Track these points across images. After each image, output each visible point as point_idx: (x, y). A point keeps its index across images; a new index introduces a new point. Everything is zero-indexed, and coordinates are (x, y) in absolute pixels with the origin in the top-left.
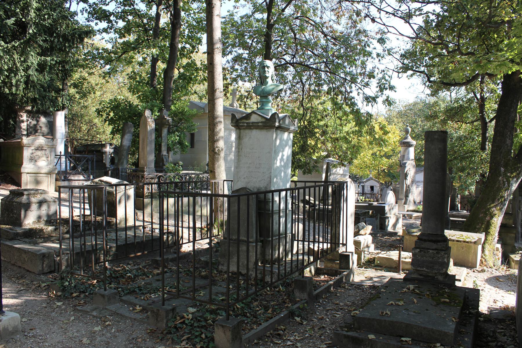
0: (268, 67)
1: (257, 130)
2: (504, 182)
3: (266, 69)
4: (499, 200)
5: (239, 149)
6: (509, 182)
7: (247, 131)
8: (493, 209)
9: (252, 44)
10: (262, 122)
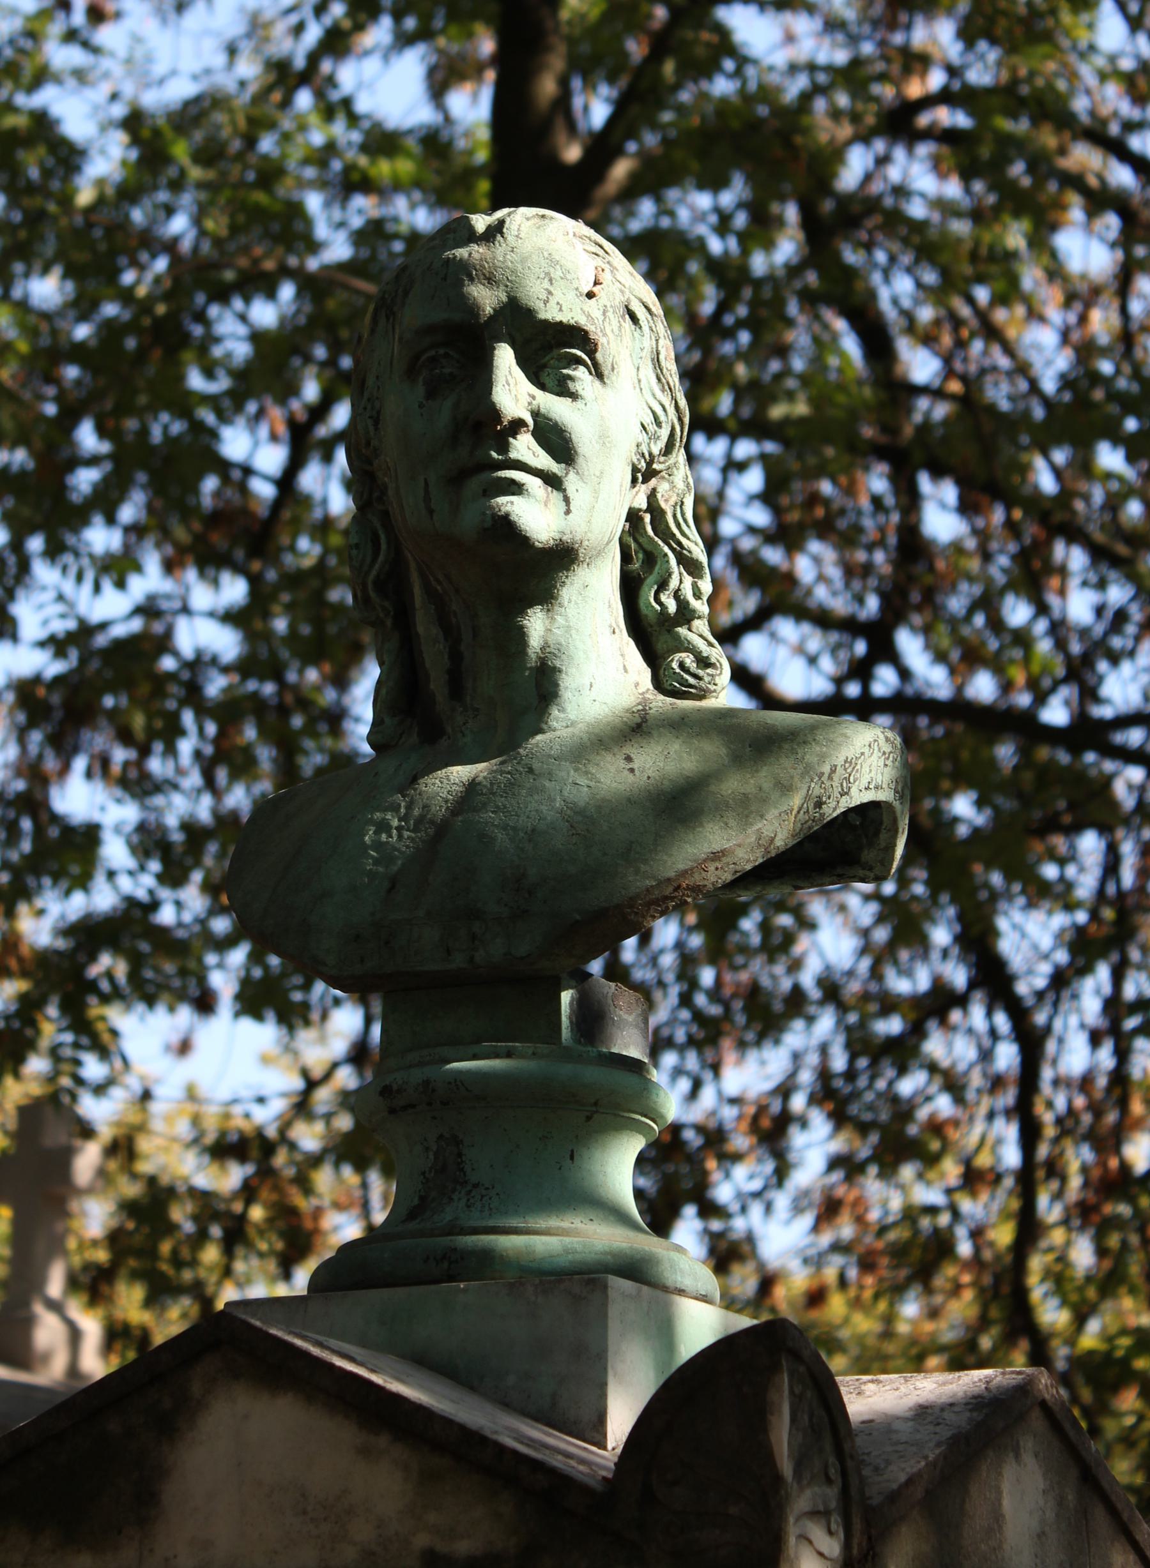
0: (556, 351)
3: (512, 390)
9: (286, 481)
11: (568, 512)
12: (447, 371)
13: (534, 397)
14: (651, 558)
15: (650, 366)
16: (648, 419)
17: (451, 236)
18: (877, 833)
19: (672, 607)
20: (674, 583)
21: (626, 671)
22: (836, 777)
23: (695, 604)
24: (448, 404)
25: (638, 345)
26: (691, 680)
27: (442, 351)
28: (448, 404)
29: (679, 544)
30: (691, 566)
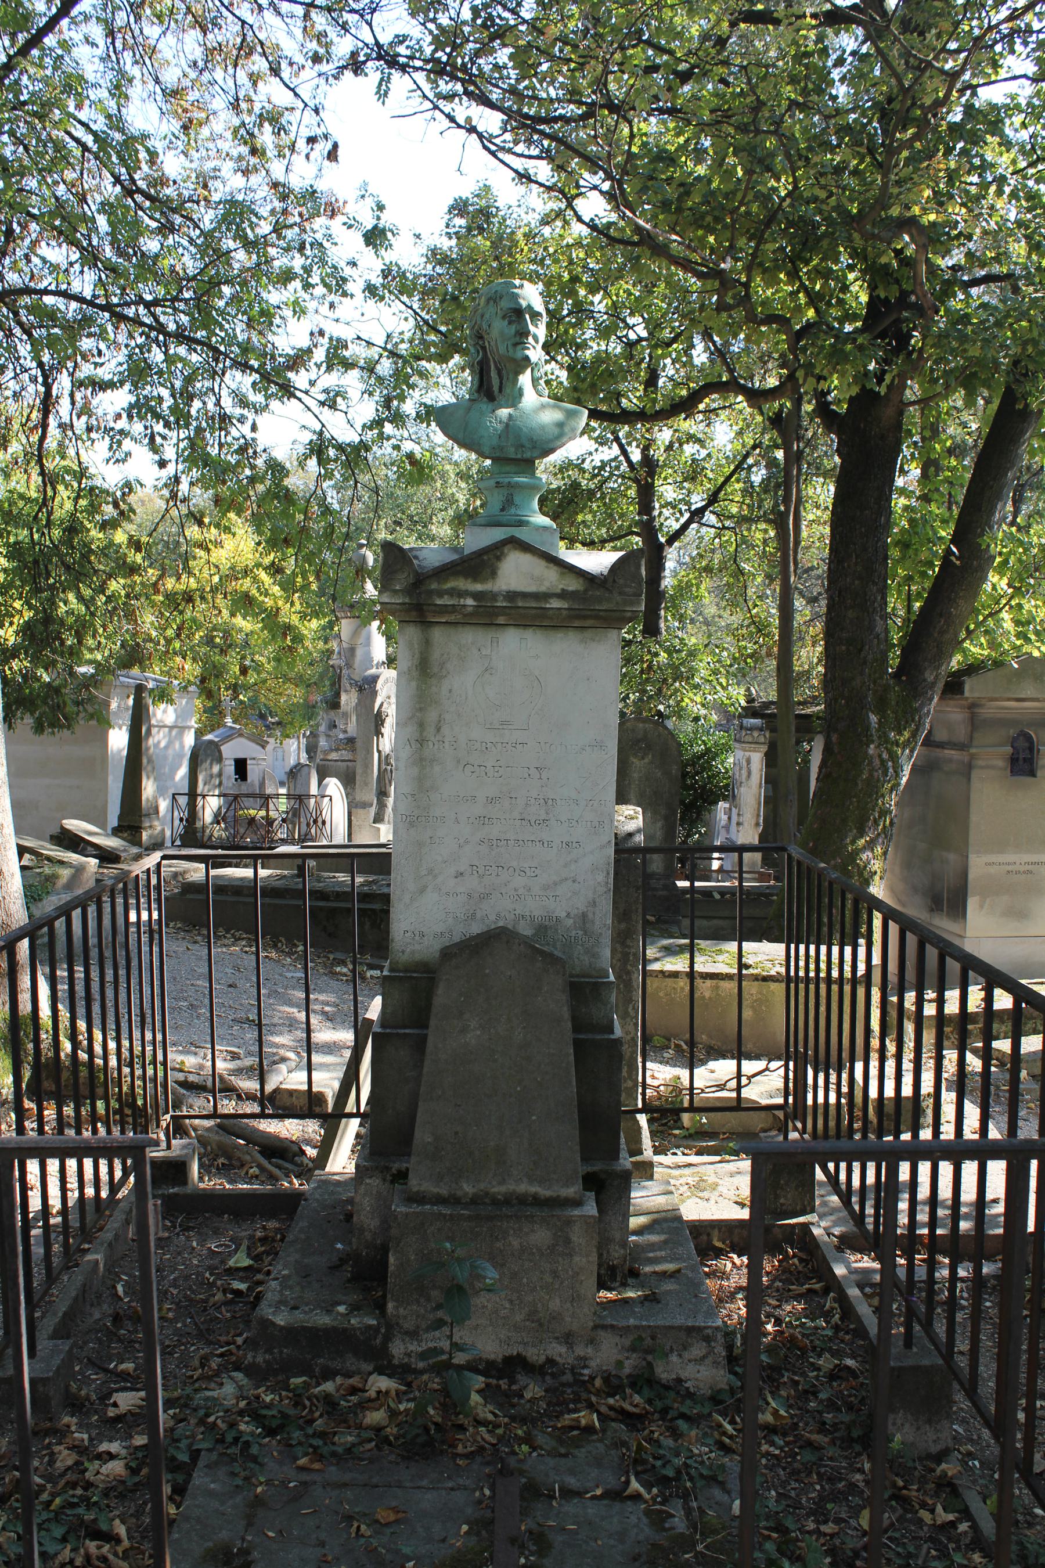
1: (529, 634)
2: (883, 762)
4: (876, 823)
5: (421, 725)
6: (894, 758)
7: (469, 636)
8: (864, 857)
10: (563, 595)
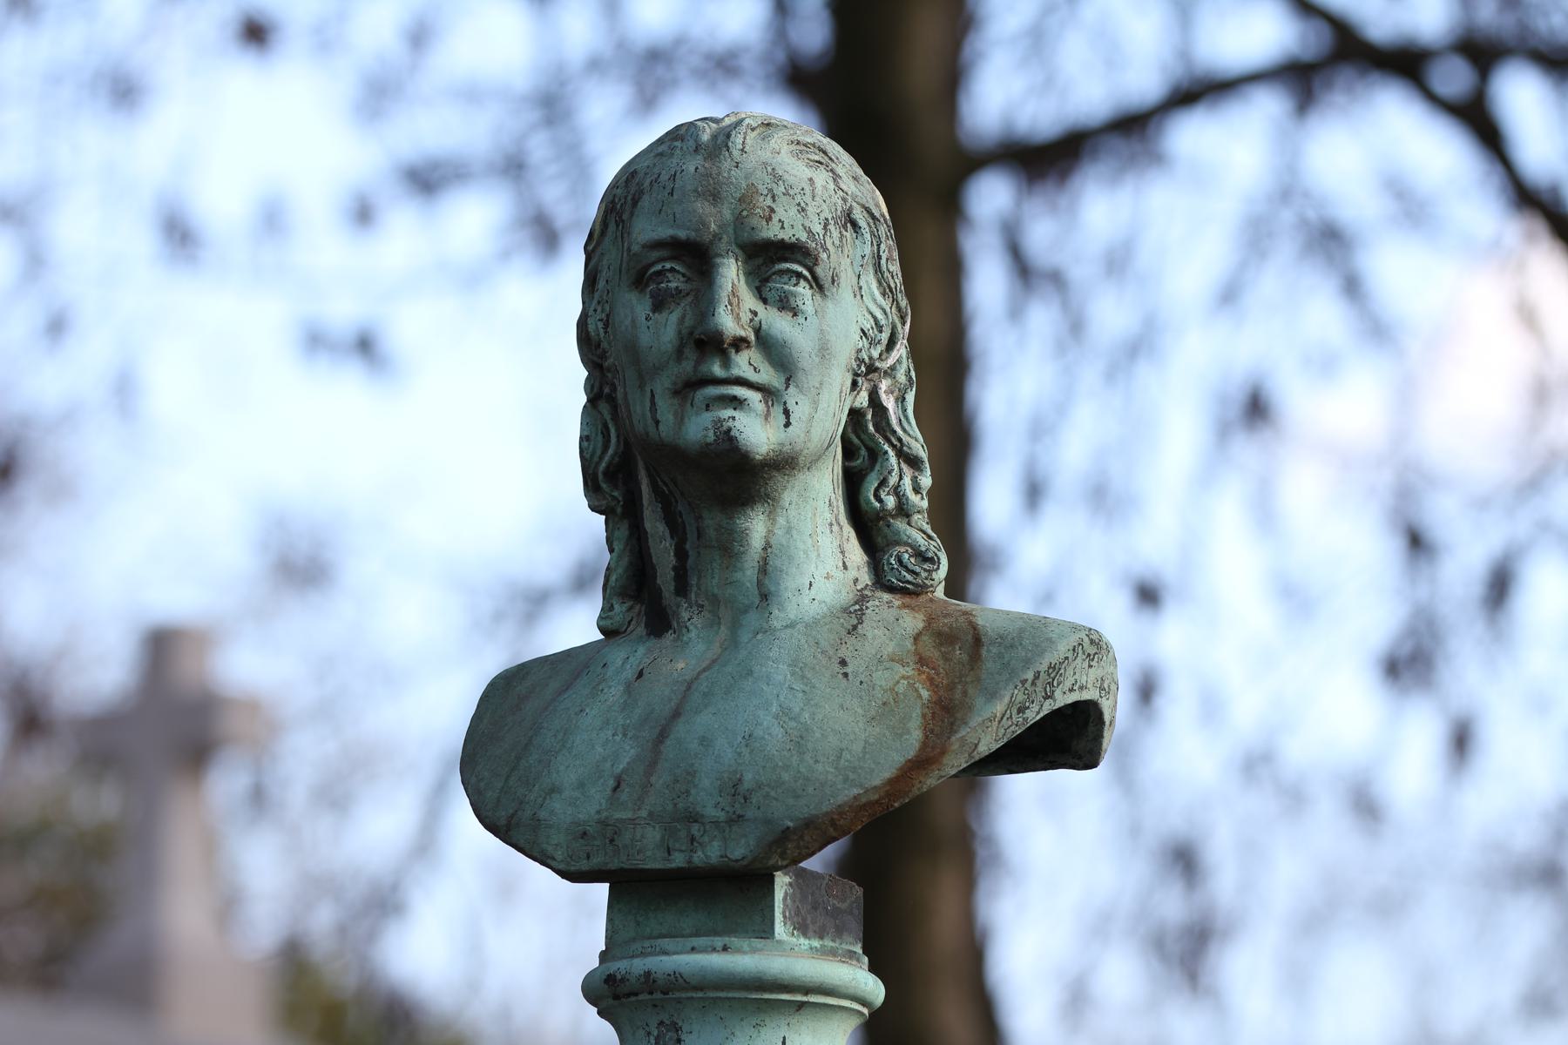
3: (735, 302)
11: (787, 424)
12: (673, 285)
13: (755, 314)
14: (875, 455)
15: (872, 271)
16: (868, 324)
17: (678, 144)
18: (1086, 724)
19: (891, 502)
20: (893, 480)
21: (845, 567)
22: (1039, 683)
23: (914, 498)
24: (674, 317)
25: (859, 253)
26: (909, 577)
27: (668, 266)
28: (674, 317)
29: (900, 440)
30: (914, 462)
